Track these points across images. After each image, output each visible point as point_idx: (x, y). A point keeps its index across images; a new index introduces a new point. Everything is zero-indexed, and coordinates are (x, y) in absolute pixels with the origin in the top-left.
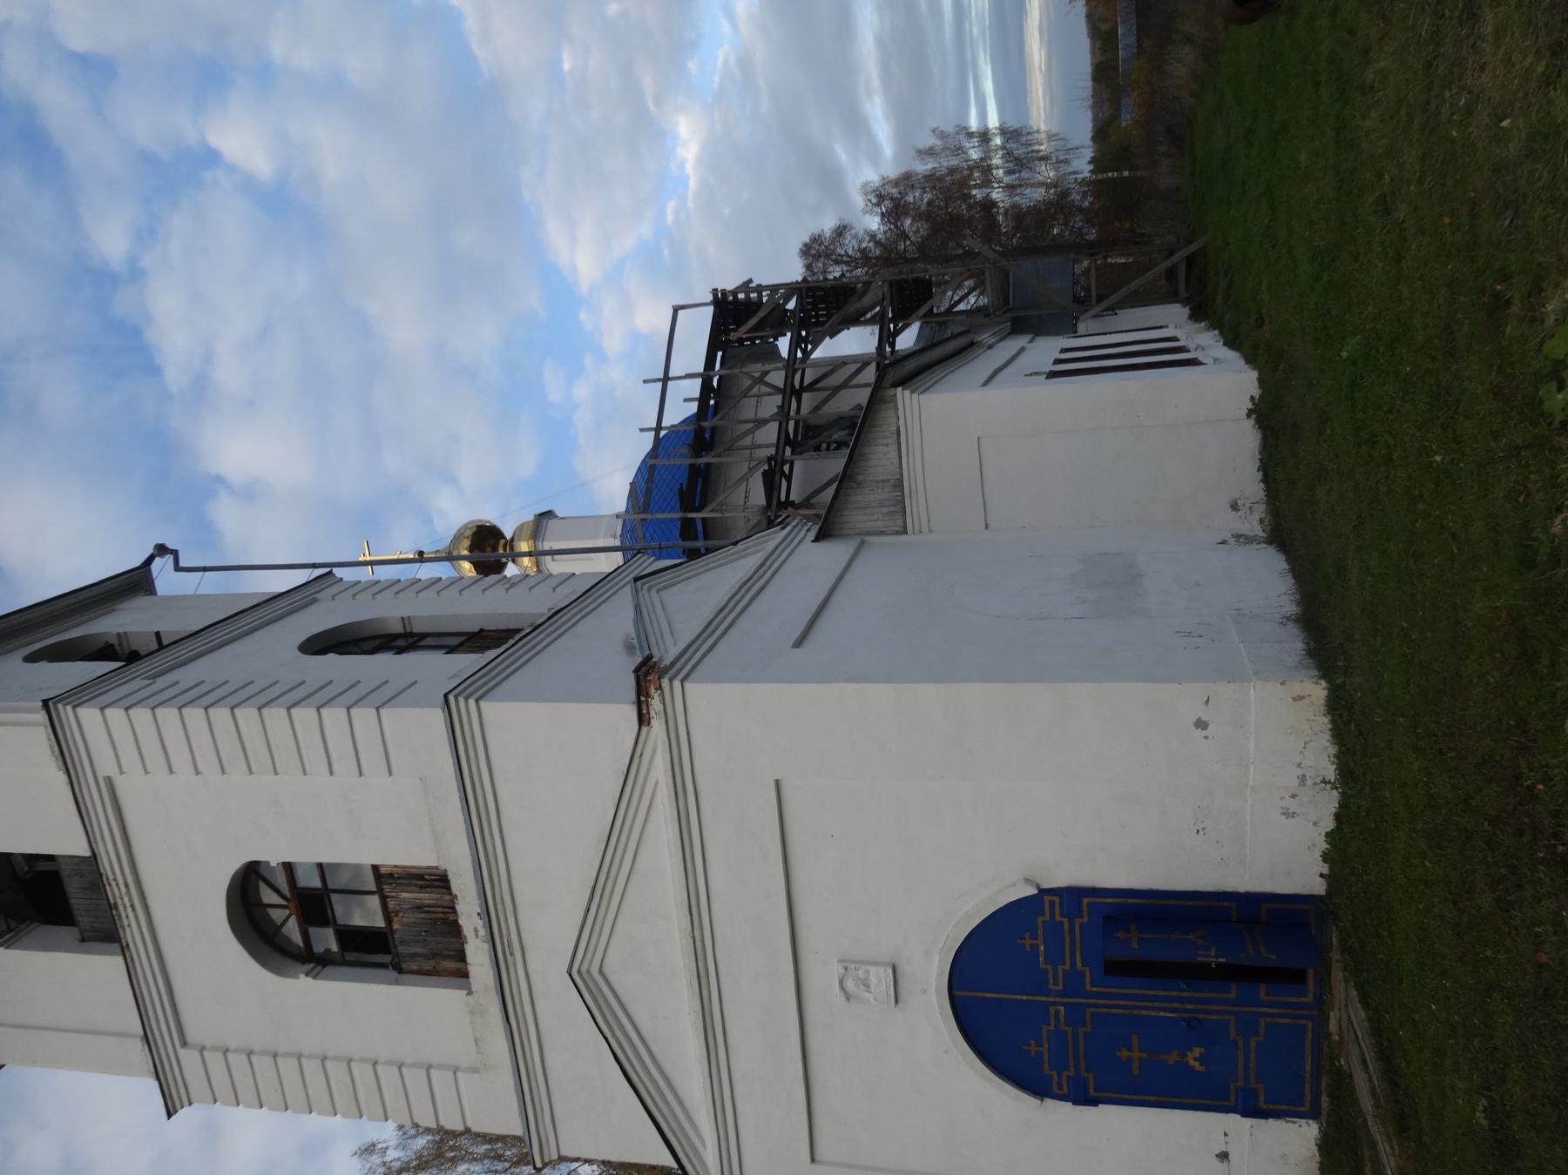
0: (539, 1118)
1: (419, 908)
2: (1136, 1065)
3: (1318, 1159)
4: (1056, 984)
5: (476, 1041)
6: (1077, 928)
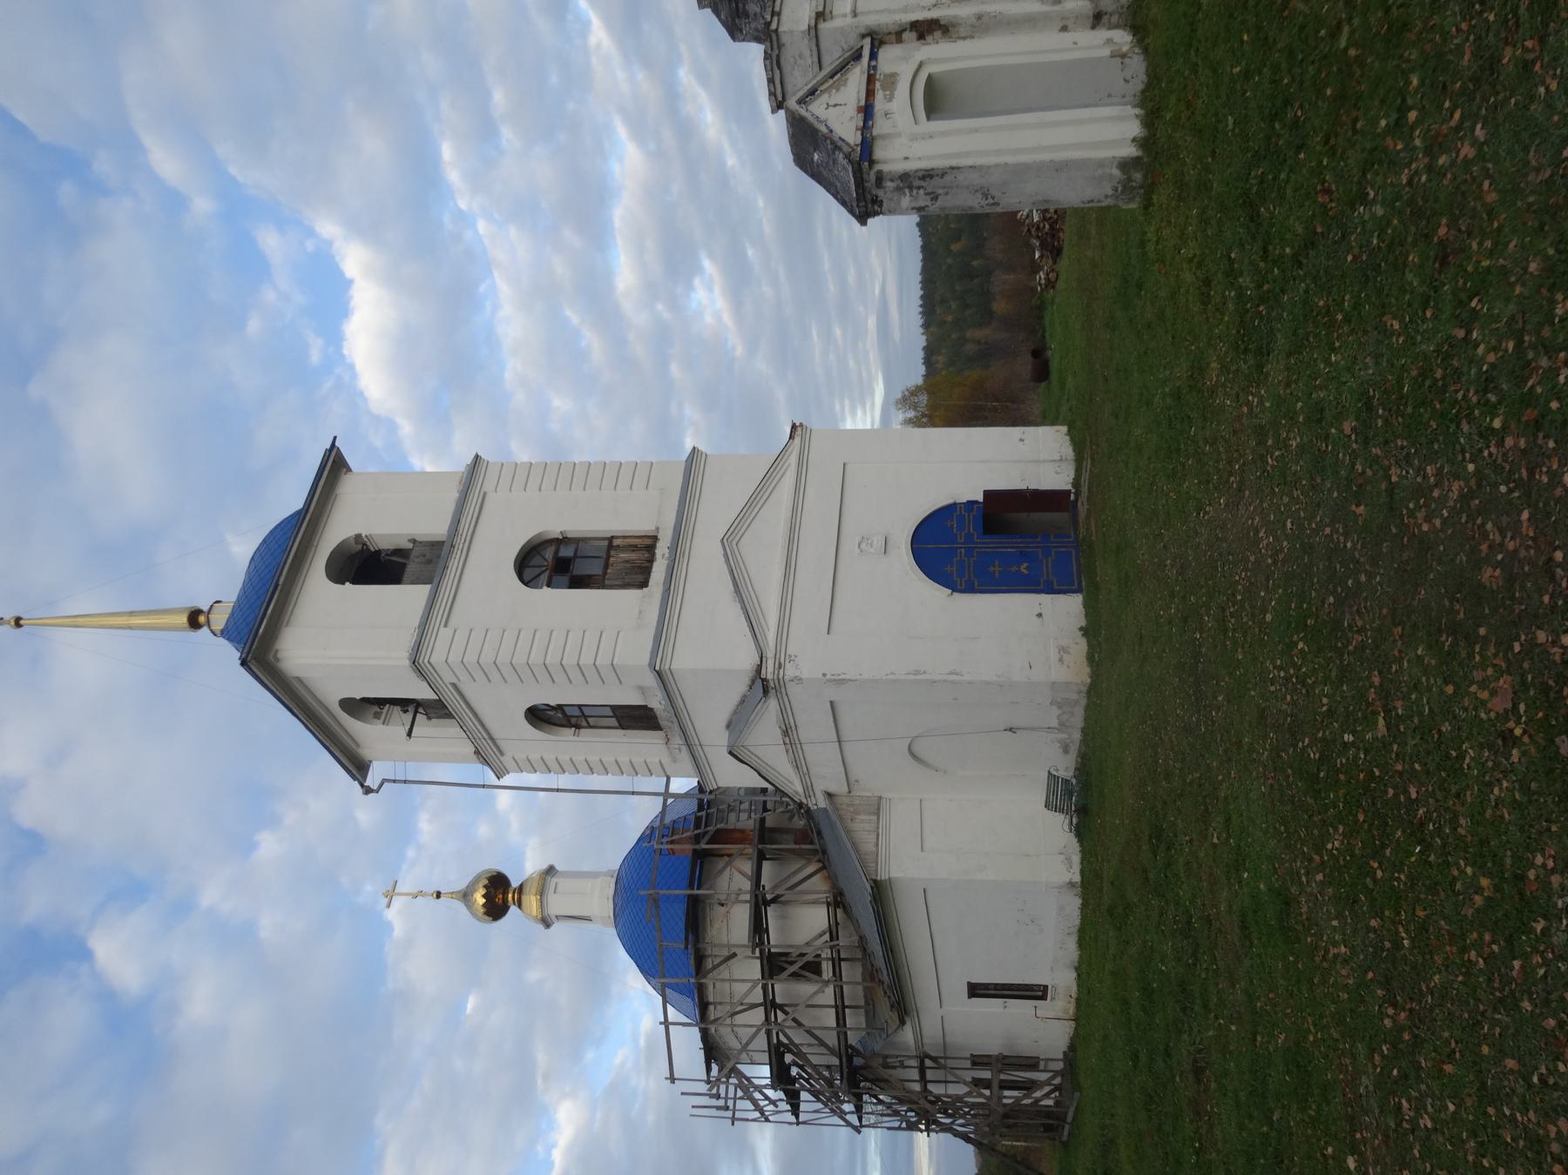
1: (627, 562)
2: (997, 574)
6: (972, 562)
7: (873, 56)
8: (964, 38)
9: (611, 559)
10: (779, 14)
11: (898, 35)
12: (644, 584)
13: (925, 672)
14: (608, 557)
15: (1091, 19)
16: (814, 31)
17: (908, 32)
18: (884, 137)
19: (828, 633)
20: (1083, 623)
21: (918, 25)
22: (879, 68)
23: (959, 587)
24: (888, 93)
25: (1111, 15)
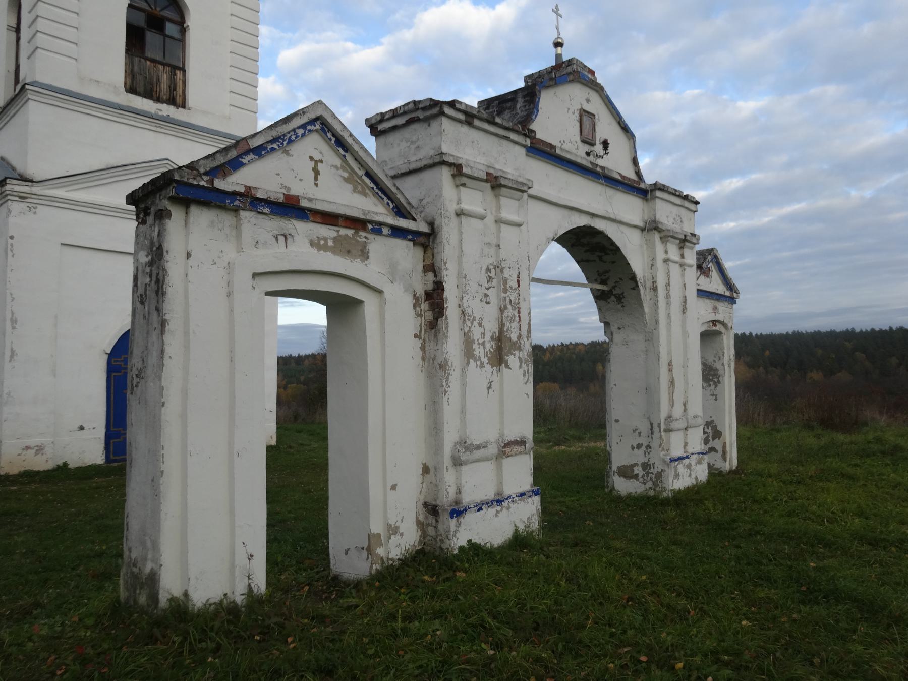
0: (59, 100)
3: (84, 465)
4: (115, 361)
5: (98, 81)
7: (398, 232)
8: (423, 348)
9: (161, 67)
10: (469, 124)
11: (431, 268)
12: (131, 89)
13: (14, 328)
14: (164, 64)
15: (434, 503)
16: (440, 162)
17: (434, 279)
18: (238, 227)
19: (62, 244)
20: (72, 465)
21: (440, 291)
22: (378, 238)
23: (113, 360)
24: (330, 243)
25: (435, 527)
